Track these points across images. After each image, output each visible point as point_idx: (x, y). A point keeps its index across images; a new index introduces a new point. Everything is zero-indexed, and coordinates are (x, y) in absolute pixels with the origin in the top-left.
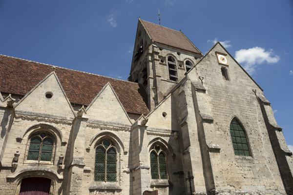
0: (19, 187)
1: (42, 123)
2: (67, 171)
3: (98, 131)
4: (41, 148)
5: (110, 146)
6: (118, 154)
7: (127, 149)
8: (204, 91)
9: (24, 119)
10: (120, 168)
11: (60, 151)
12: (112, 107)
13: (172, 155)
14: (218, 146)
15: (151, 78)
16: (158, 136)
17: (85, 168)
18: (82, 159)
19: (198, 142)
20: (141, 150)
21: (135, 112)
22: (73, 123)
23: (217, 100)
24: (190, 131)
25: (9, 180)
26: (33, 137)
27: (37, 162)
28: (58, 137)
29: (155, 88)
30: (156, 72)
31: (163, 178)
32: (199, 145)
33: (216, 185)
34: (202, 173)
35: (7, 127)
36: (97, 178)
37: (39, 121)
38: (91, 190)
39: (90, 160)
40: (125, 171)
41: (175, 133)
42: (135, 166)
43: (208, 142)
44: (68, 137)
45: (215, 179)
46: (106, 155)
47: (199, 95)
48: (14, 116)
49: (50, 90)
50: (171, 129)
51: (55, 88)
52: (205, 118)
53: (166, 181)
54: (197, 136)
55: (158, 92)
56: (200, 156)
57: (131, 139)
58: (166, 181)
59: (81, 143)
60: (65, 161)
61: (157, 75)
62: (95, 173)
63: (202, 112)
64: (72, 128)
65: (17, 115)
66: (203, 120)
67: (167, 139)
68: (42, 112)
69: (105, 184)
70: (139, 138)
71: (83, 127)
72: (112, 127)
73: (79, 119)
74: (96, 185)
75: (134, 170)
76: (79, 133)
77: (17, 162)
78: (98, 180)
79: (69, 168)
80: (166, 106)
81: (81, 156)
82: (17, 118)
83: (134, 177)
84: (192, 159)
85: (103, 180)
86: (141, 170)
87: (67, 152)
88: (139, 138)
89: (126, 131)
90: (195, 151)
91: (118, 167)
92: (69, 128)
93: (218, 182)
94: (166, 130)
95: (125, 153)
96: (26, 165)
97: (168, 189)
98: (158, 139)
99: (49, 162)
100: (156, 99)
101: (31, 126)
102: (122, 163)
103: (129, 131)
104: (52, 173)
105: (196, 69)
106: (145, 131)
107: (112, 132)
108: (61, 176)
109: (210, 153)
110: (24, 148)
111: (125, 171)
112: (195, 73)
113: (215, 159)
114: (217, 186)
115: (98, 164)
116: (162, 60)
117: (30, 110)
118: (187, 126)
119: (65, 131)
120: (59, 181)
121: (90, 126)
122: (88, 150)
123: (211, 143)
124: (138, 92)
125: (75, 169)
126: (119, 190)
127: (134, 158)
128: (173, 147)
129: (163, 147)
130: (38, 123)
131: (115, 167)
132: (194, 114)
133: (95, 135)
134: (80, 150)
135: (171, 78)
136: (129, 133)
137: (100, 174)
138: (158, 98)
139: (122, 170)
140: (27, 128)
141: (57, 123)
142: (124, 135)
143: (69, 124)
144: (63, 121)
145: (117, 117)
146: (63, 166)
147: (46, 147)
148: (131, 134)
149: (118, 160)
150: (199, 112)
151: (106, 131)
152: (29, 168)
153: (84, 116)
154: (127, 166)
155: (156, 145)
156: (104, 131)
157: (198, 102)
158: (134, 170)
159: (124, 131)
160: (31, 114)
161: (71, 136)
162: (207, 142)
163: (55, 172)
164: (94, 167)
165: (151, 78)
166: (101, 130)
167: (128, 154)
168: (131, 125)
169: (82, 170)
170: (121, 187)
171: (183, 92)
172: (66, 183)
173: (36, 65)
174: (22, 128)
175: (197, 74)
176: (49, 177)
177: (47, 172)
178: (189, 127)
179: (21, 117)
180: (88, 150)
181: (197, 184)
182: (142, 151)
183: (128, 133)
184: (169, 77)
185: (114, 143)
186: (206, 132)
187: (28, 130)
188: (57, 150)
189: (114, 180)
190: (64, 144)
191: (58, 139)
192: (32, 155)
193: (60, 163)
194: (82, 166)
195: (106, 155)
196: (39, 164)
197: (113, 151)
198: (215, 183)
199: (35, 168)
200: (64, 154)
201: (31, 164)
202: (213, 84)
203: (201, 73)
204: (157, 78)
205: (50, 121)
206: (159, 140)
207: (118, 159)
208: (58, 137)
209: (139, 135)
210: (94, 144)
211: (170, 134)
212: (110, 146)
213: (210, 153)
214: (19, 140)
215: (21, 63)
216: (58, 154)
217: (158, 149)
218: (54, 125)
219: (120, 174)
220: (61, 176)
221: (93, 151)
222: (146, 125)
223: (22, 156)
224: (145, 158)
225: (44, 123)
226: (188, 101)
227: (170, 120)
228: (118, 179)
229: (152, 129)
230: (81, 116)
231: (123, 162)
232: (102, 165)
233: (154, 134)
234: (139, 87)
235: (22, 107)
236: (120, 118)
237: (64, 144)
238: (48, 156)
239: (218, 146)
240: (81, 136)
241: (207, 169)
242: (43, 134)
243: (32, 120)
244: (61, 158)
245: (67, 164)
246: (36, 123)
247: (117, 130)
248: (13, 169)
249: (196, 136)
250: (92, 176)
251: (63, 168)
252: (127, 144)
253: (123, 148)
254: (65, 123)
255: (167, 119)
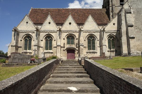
0: (66, 52)
1: (69, 33)
2: (79, 47)
3: (88, 34)
4: (70, 41)
5: (93, 38)
6: (95, 41)
7: (99, 39)
8: (130, 13)
9: (64, 32)
10: (96, 46)
11: (76, 41)
12: (92, 24)
13: (117, 40)
14: (134, 36)
15: (110, 6)
16: (111, 33)
17: (84, 46)
18: (83, 43)
19: (126, 35)
20: (103, 39)
21: (104, 23)
22: (79, 32)
23: (138, 15)
24: (122, 31)
25: (64, 50)
26: (68, 38)
27: (70, 45)
28: (75, 37)
29: (112, 11)
30: (113, 3)
31: (113, 48)
32: (126, 36)
33: (131, 50)
34: (127, 46)
35: (60, 36)
36: (89, 49)
37: (68, 32)
38: (87, 53)
39: (86, 44)
40: (98, 47)
41: (118, 31)
42: (101, 45)
43: (129, 35)
44: (78, 37)
45: (131, 49)
46: (91, 41)
47: (128, 15)
48: (61, 32)
49: (70, 22)
50: (117, 30)
51: (72, 20)
52: (129, 25)
53: (114, 49)
54: (126, 33)
55: (114, 13)
56: (126, 40)
57: (100, 35)
58: (114, 49)
59: (82, 39)
60: (78, 44)
61: (113, 5)
62: (88, 47)
63: (128, 22)
64: (79, 33)
65: (62, 32)
66: (129, 26)
67: (115, 34)
68: (69, 30)
69: (92, 51)
70: (102, 35)
71: (82, 33)
72: (93, 32)
73: (80, 31)
74: (88, 51)
75: (101, 46)
76: (81, 36)
77: (65, 45)
78: (89, 50)
79: (79, 46)
80: (115, 20)
81: (82, 43)
82: (62, 32)
83: (101, 49)
84: (122, 42)
85: (91, 50)
86: (103, 46)
87: (78, 42)
88: (102, 35)
89: (98, 32)
90: (124, 39)
91: (96, 45)
92: (78, 34)
93: (132, 50)
94: (115, 30)
95: (98, 40)
96: (67, 46)
97: (115, 52)
98: (111, 34)
99: (73, 45)
100: (112, 16)
101: (66, 34)
102: (97, 44)
103: (100, 32)
104: (75, 48)
105: (128, 2)
106: (105, 32)
107: (93, 33)
108: (77, 49)
109: (130, 39)
110: (66, 41)
111: (98, 47)
112: (127, 4)
113: (131, 41)
114: (132, 51)
115: (89, 45)
116: (36, 62)
117: (65, 29)
118: (121, 29)
119: (77, 35)
120: (77, 50)
121: (85, 32)
122: (85, 40)
123: (131, 35)
124: (105, 13)
125: (81, 47)
126: (96, 53)
127: (101, 42)
128: (118, 37)
129: (113, 37)
130: (68, 33)
131: (95, 45)
132: (125, 23)
133: (87, 35)
134: (82, 41)
135: (121, 4)
136: (99, 33)
137: (90, 48)
138: (114, 16)
139: (97, 46)
140: (66, 35)
141: (74, 32)
142: (97, 34)
143: (78, 32)
144: (76, 32)
145: (94, 28)
146: (78, 46)
147: (72, 40)
148: (100, 34)
149: (96, 43)
150: (127, 22)
151: (91, 33)
152: (68, 47)
153: (82, 30)
154: (99, 45)
155: (110, 37)
156: (90, 33)
157: (127, 18)
158: (101, 46)
159: (97, 33)
160: (66, 31)
161: (79, 36)
162: (129, 34)
163: (76, 48)
164: (87, 45)
165: (110, 6)
166: (89, 33)
167: (99, 41)
168: (100, 30)
169: (83, 47)
170: (97, 52)
171: (121, 14)
172: (79, 51)
173: (64, 10)
174: (64, 35)
175: (128, 4)
176: (74, 49)
177: (73, 48)
178: (122, 29)
179: (63, 32)
180: (85, 40)
181: (124, 51)
182: (103, 40)
183: (99, 33)
184: (120, 4)
185: (94, 37)
186: (129, 31)
187: (66, 36)
188: (75, 41)
189: (95, 50)
190: (77, 39)
191: (75, 38)
192: (68, 43)
193: (76, 45)
194: (83, 46)
195: (91, 41)
196: (71, 46)
197: (94, 40)
198: (131, 50)
199: (70, 47)
200: (77, 42)
201: (69, 46)
202: (137, 8)
203: (130, 4)
204: (113, 6)
205: (72, 32)
206: (112, 35)
207: (95, 42)
208: (75, 37)
209: (102, 34)
210: (87, 38)
211: (116, 32)
212: (93, 38)
213: (130, 39)
214: (64, 39)
215: (59, 10)
216: (76, 42)
217: (111, 38)
218: (73, 33)
219: (96, 47)
220: (77, 49)
221: (87, 41)
222: (105, 30)
223: (66, 44)
224: (106, 42)
225: (70, 33)
226: (122, 19)
227: (117, 26)
228: (96, 49)
229: (108, 30)
230: (81, 30)
231: (97, 43)
232: (90, 45)
233: (109, 33)
234: (106, 11)
235: (64, 28)
236: (95, 28)
237: (77, 39)
238: (73, 43)
239: (134, 36)
240: (82, 36)
241: (128, 45)
242: (70, 37)
243: (66, 32)
244: (77, 44)
245: (79, 45)
246: (68, 33)
247: (95, 33)
248: (64, 47)
249: (125, 33)
250: (87, 48)
251: (78, 46)
252: (98, 37)
253: (97, 39)
254: (76, 32)
255: (115, 26)
